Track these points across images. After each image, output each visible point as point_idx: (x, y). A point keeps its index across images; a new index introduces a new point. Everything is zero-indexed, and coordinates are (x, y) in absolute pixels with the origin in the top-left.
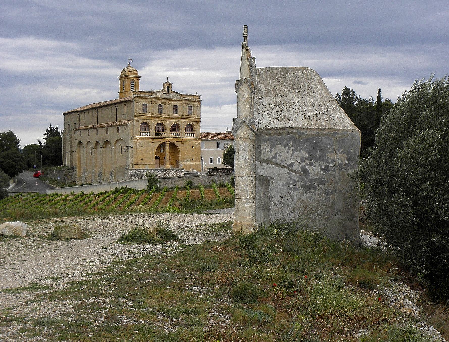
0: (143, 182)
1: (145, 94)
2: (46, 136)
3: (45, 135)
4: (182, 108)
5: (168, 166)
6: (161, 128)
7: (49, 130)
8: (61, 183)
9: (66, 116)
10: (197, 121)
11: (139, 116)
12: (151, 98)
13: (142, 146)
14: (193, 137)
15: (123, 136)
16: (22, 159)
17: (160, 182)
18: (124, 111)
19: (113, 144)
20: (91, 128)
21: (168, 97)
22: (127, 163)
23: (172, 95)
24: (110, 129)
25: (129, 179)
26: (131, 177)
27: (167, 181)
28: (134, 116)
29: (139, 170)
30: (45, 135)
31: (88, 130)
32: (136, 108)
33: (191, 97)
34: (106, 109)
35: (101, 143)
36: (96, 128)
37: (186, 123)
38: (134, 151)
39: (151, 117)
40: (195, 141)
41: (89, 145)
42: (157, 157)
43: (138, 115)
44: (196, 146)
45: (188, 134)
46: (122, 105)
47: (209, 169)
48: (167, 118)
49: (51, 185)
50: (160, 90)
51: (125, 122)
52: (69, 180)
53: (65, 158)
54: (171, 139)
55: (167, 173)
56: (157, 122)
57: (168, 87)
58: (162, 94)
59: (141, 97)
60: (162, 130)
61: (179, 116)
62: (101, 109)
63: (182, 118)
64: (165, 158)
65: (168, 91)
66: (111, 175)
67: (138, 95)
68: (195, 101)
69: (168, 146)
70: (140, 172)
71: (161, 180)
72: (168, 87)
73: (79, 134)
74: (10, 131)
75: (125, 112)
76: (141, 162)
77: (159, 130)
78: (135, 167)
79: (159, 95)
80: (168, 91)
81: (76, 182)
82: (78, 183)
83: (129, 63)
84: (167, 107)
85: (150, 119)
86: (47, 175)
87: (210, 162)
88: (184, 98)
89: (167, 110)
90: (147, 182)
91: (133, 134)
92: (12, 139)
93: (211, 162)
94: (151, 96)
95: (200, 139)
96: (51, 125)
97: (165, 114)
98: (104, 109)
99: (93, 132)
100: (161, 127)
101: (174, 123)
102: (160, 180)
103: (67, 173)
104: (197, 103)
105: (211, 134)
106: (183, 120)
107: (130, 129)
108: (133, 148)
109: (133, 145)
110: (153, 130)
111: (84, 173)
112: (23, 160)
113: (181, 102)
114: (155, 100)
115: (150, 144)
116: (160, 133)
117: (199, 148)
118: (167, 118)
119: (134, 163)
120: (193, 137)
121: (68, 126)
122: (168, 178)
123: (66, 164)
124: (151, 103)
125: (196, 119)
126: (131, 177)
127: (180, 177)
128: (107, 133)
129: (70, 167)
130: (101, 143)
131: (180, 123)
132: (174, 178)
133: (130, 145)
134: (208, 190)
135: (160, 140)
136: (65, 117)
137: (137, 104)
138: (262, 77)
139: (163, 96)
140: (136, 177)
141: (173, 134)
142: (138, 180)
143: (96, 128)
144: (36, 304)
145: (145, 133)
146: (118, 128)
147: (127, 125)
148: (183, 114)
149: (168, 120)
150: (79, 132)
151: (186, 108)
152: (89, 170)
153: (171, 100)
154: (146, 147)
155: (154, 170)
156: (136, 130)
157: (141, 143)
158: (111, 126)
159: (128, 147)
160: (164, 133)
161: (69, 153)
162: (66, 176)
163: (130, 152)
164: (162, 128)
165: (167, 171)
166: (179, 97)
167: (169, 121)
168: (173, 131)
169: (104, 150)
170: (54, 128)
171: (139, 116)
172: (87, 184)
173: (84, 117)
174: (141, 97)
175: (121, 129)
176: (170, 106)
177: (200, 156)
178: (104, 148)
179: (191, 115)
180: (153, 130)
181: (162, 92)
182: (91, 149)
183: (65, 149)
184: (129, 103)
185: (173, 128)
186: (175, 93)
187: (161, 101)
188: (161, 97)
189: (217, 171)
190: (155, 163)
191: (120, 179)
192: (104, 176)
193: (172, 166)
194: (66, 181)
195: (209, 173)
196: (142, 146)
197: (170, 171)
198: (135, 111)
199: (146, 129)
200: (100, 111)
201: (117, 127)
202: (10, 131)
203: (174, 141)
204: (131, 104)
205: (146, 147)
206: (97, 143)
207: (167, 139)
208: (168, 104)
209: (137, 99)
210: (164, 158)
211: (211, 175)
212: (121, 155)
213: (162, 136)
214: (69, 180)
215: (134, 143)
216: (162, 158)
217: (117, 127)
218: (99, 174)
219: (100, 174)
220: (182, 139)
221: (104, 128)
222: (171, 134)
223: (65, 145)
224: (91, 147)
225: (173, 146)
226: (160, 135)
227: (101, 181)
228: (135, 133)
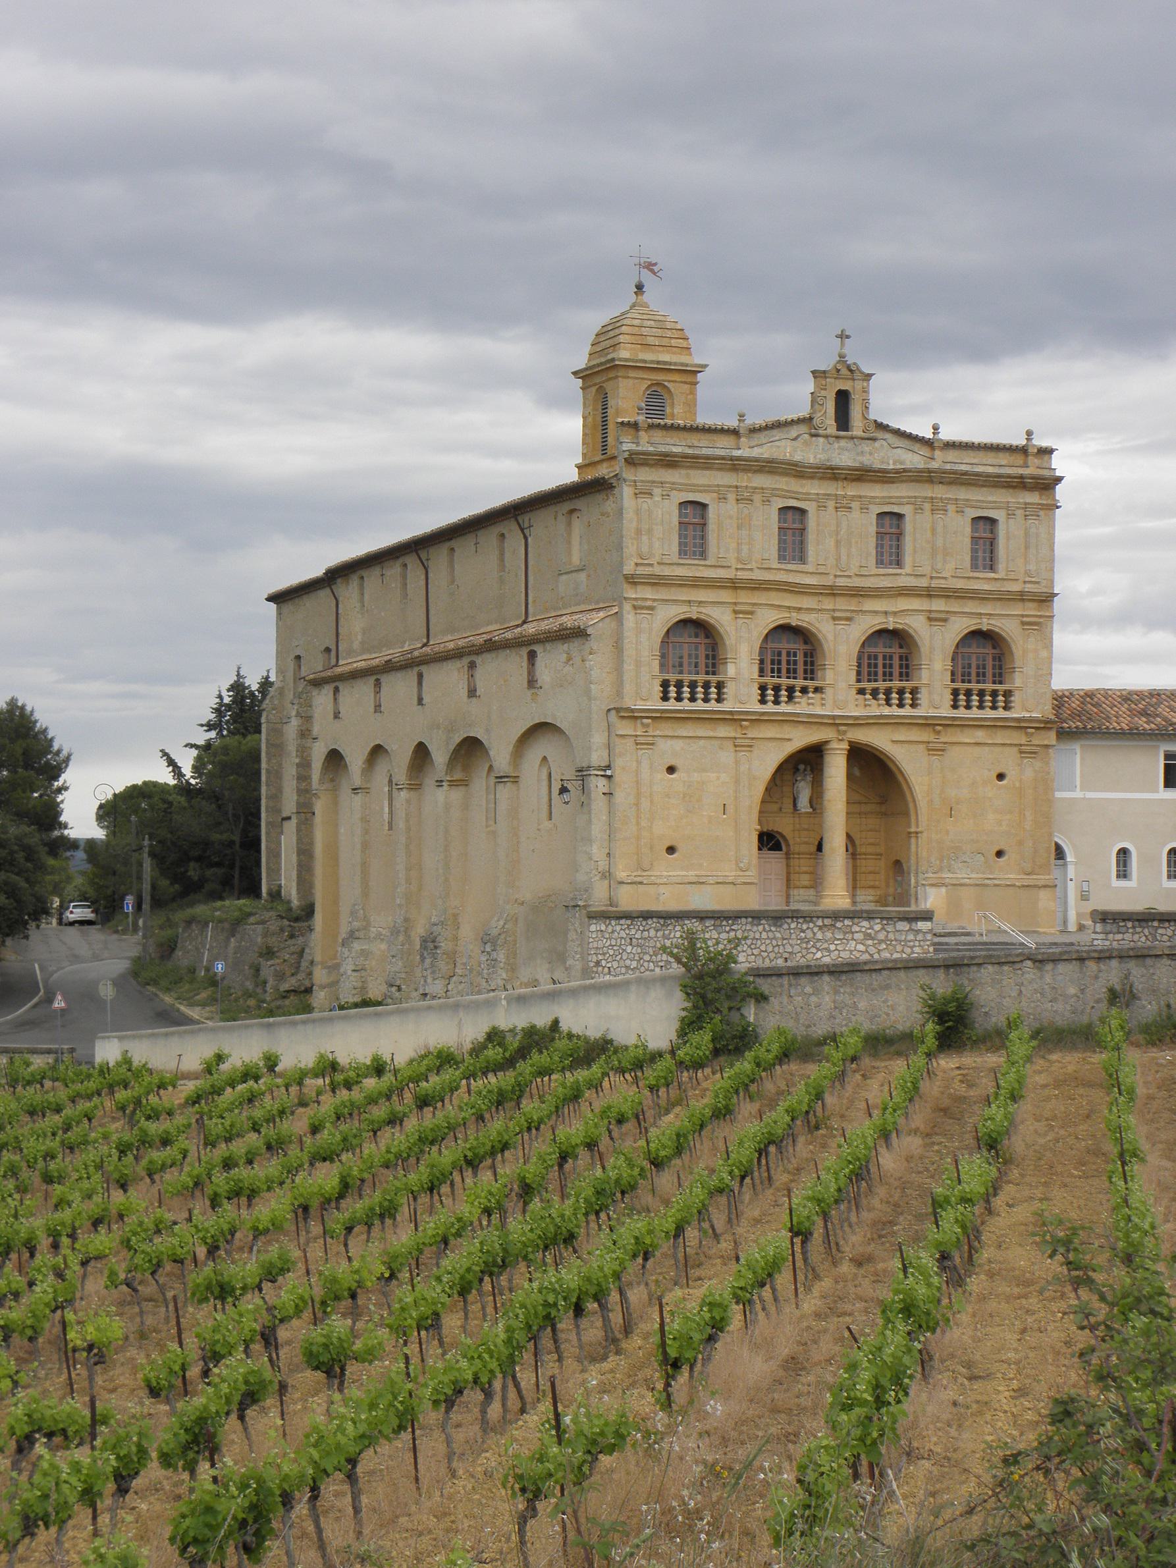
0: (657, 993)
1: (694, 439)
2: (213, 734)
3: (210, 726)
4: (933, 530)
5: (837, 895)
6: (800, 658)
7: (227, 700)
8: (236, 1000)
9: (288, 608)
10: (1031, 610)
11: (657, 582)
12: (735, 465)
13: (671, 770)
14: (1001, 713)
15: (557, 710)
16: (20, 856)
17: (761, 998)
18: (570, 554)
19: (500, 753)
20: (389, 667)
21: (844, 456)
22: (581, 877)
23: (866, 447)
24: (490, 669)
25: (586, 973)
26: (598, 963)
27: (808, 989)
28: (626, 577)
29: (646, 916)
30: (210, 726)
31: (372, 680)
32: (639, 532)
33: (991, 458)
34: (473, 548)
35: (440, 756)
36: (413, 664)
37: (960, 626)
38: (619, 797)
39: (734, 585)
40: (1019, 738)
41: (382, 769)
42: (769, 841)
44: (1022, 772)
45: (968, 693)
46: (560, 517)
47: (1104, 917)
48: (832, 592)
49: (182, 1008)
50: (795, 416)
51: (568, 621)
52: (280, 976)
53: (275, 855)
55: (819, 935)
56: (769, 619)
57: (843, 398)
58: (806, 443)
59: (668, 461)
60: (800, 668)
63: (929, 593)
64: (820, 848)
65: (843, 420)
66: (488, 948)
67: (651, 449)
68: (1020, 484)
69: (836, 769)
70: (652, 933)
71: (769, 980)
72: (843, 398)
73: (330, 707)
74: (12, 703)
75: (576, 560)
76: (666, 870)
77: (784, 671)
78: (628, 900)
79: (783, 448)
80: (843, 420)
81: (308, 991)
82: (319, 997)
83: (640, 288)
84: (838, 525)
85: (725, 596)
86: (173, 950)
87: (1118, 876)
88: (948, 467)
89: (838, 543)
90: (679, 995)
91: (619, 693)
92: (19, 751)
93: (1123, 874)
95: (1045, 725)
96: (238, 675)
97: (822, 569)
98: (464, 546)
99: (399, 687)
101: (877, 623)
102: (765, 986)
103: (273, 941)
104: (1033, 498)
105: (1128, 697)
106: (938, 605)
107: (598, 661)
108: (617, 779)
109: (618, 763)
111: (352, 936)
112: (28, 859)
113: (927, 491)
115: (727, 756)
117: (1044, 786)
118: (832, 592)
119: (622, 875)
120: (1001, 713)
121: (291, 665)
122: (814, 972)
123: (280, 886)
124: (731, 497)
125: (1021, 597)
126: (598, 963)
127: (894, 967)
128: (472, 693)
129: (295, 903)
130: (440, 756)
131: (917, 625)
133: (597, 757)
134: (1067, 1061)
135: (788, 731)
137: (645, 503)
139: (812, 453)
140: (628, 962)
142: (627, 983)
143: (413, 664)
145: (693, 685)
146: (532, 655)
147: (579, 633)
148: (939, 566)
149: (842, 604)
150: (328, 690)
151: (959, 529)
152: (381, 922)
153: (862, 475)
154: (696, 777)
155: (736, 916)
156: (638, 664)
157: (670, 748)
158: (491, 647)
159: (582, 773)
160: (817, 690)
161: (294, 821)
162: (269, 953)
163: (599, 804)
164: (805, 655)
165: (820, 923)
166: (914, 459)
167: (848, 614)
168: (873, 676)
169: (456, 795)
170: (255, 687)
171: (657, 582)
172: (366, 1003)
173: (358, 605)
174: (668, 461)
175: (550, 662)
176: (856, 514)
177: (1051, 835)
178: (453, 784)
179: (992, 575)
181: (803, 429)
182: (390, 792)
183: (276, 797)
184: (600, 497)
185: (876, 658)
186: (888, 436)
187: (794, 485)
188: (797, 457)
189: (1157, 928)
190: (752, 874)
191: (542, 973)
192: (452, 957)
193: (866, 899)
194: (265, 982)
195: (1097, 939)
196: (671, 770)
197: (839, 925)
198: (630, 548)
200: (438, 557)
201: (524, 652)
202: (12, 703)
203: (879, 739)
204: (609, 506)
205: (696, 777)
206: (421, 753)
207: (834, 723)
208: (843, 506)
209: (644, 475)
210: (814, 848)
211: (1103, 956)
212: (547, 824)
213: (802, 706)
214: (280, 976)
215: (620, 745)
216: (803, 848)
217: (524, 652)
218: (424, 941)
219: (430, 943)
220: (928, 724)
222: (861, 692)
223: (276, 774)
224: (390, 781)
226: (790, 698)
227: (436, 987)
228: (628, 688)
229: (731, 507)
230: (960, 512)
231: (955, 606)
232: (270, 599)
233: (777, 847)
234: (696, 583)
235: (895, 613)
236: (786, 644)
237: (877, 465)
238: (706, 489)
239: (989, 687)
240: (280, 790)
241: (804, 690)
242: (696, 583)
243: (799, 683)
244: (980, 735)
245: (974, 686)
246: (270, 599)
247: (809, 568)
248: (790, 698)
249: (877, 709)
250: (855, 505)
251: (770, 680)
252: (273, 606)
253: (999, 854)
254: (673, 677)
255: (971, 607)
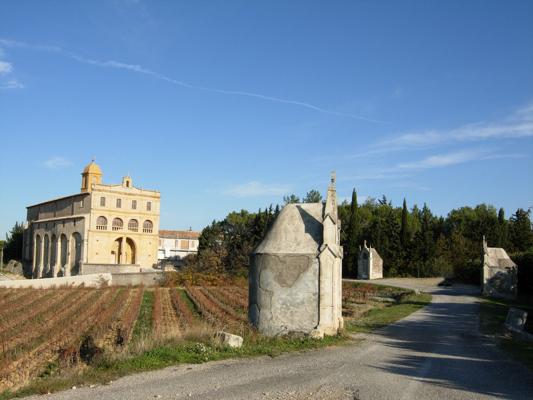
4: (141, 204)
12: (110, 192)
29: (93, 264)
32: (94, 202)
35: (156, 229)
43: (95, 208)
53: (25, 252)
54: (128, 234)
61: (138, 212)
62: (60, 202)
85: (108, 212)
94: (110, 190)
100: (119, 222)
110: (110, 225)
114: (114, 194)
116: (117, 228)
124: (109, 197)
132: (128, 274)
136: (28, 210)
137: (95, 197)
138: (344, 340)
141: (131, 229)
144: (9, 389)
153: (130, 194)
160: (122, 228)
161: (29, 246)
168: (130, 227)
171: (143, 214)
180: (110, 225)
183: (26, 241)
199: (103, 223)
208: (127, 199)
221: (62, 221)
222: (129, 229)
225: (130, 242)
226: (117, 230)
229: (109, 198)
230: (145, 201)
231: (144, 216)
232: (26, 208)
233: (114, 254)
234: (103, 210)
235: (134, 217)
236: (117, 221)
237: (133, 193)
238: (105, 195)
239: (149, 229)
240: (26, 241)
241: (120, 228)
242: (103, 210)
243: (119, 227)
244: (147, 236)
245: (147, 229)
246: (26, 208)
247: (121, 209)
248: (117, 230)
249: (131, 232)
250: (129, 199)
251: (114, 227)
252: (27, 209)
253: (150, 256)
254: (145, 229)
255: (146, 216)
